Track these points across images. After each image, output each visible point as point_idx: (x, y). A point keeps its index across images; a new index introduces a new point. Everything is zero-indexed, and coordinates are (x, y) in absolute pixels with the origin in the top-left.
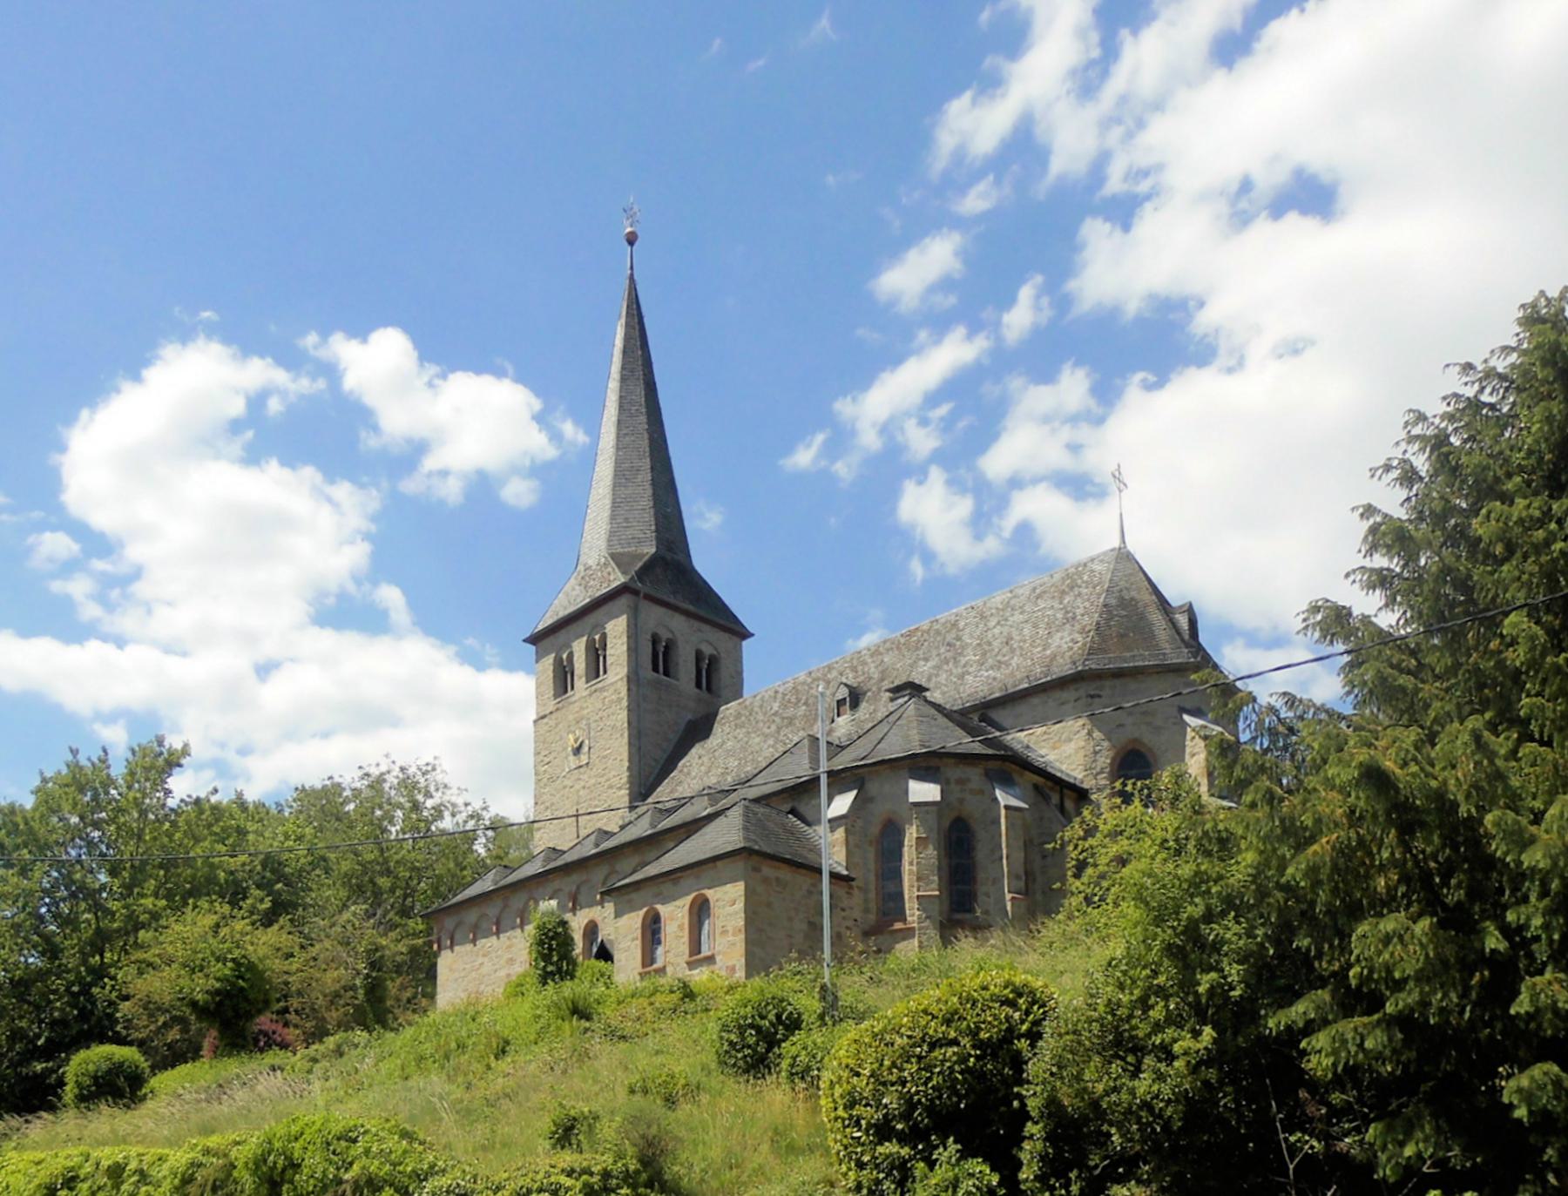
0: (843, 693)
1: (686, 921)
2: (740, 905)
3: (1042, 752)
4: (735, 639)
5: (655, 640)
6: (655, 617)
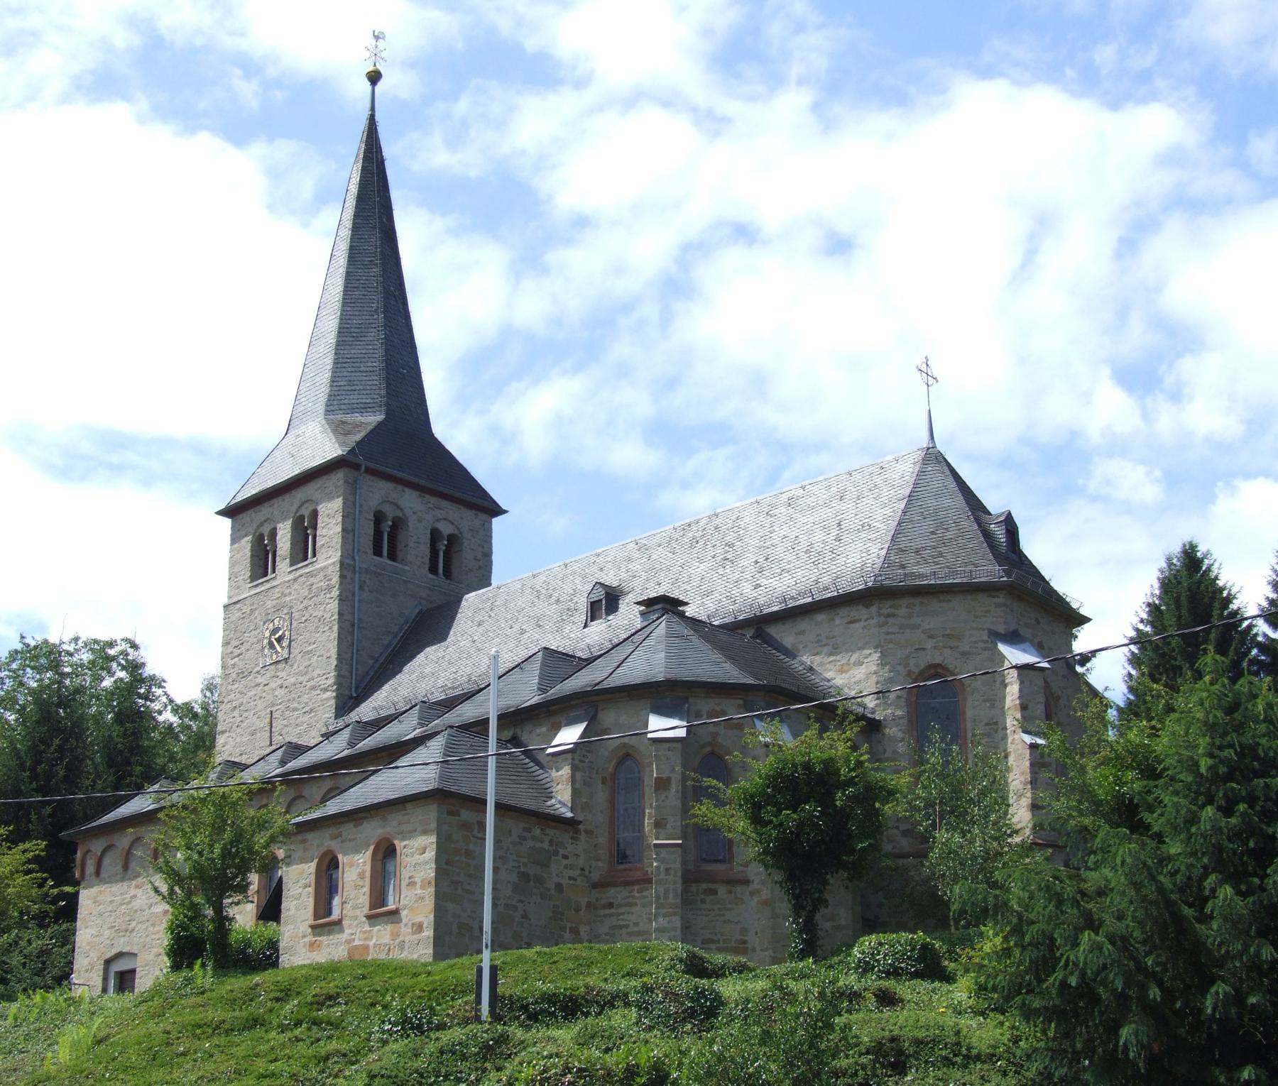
0: (600, 594)
1: (368, 868)
2: (431, 854)
3: (829, 675)
4: (484, 517)
5: (379, 518)
6: (377, 493)
